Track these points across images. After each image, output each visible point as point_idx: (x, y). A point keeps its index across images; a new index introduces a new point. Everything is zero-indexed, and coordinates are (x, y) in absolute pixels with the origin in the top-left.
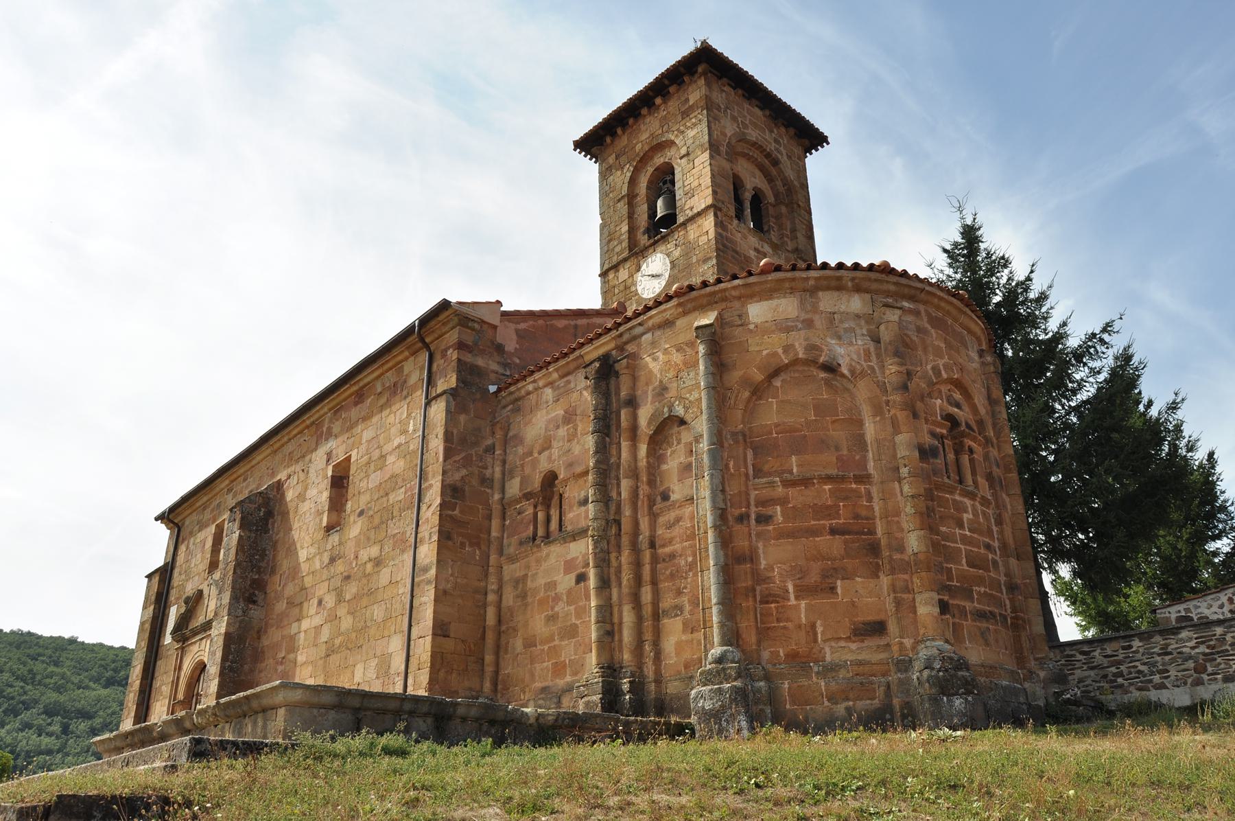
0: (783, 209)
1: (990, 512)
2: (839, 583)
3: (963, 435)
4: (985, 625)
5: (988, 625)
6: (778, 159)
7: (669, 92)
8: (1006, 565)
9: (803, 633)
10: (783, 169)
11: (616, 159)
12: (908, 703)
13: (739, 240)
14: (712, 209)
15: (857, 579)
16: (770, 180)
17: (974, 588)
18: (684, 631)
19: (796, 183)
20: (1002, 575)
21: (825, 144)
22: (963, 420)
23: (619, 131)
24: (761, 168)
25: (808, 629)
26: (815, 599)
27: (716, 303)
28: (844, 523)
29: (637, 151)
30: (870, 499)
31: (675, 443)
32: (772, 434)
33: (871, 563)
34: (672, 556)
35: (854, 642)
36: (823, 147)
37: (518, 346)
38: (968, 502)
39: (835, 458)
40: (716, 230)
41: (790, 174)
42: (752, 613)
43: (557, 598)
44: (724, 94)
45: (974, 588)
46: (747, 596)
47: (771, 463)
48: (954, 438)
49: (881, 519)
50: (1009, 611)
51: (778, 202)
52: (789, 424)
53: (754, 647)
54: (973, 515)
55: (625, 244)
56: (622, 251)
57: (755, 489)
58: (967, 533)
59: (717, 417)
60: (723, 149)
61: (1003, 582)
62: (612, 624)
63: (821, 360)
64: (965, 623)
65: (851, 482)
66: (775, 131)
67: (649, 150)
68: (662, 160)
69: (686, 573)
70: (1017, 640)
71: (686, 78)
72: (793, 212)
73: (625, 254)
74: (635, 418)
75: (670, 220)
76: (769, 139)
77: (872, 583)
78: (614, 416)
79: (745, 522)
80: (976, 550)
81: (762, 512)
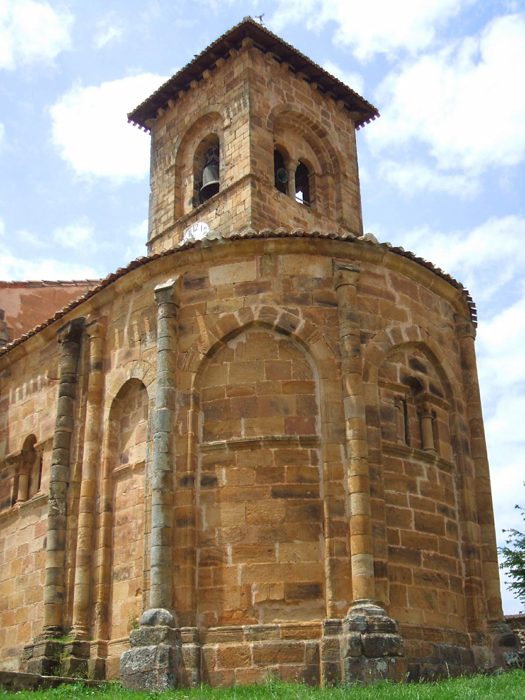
0: (330, 180)
1: (453, 476)
2: (277, 546)
3: (426, 398)
4: (431, 588)
5: (435, 588)
6: (325, 130)
7: (216, 66)
8: (464, 528)
9: (237, 595)
10: (330, 140)
11: (167, 131)
12: (333, 665)
13: (277, 209)
14: (250, 180)
15: (296, 541)
16: (317, 151)
17: (422, 551)
18: (130, 594)
19: (344, 154)
20: (460, 538)
21: (375, 116)
22: (427, 383)
23: (170, 103)
24: (309, 140)
25: (244, 591)
26: (252, 562)
27: (180, 266)
28: (287, 486)
29: (186, 122)
30: (315, 461)
31: (137, 406)
32: (223, 396)
33: (311, 526)
34: (125, 519)
35: (288, 604)
36: (374, 119)
37: (22, 312)
38: (424, 466)
39: (283, 420)
40: (252, 200)
41: (338, 145)
42: (189, 576)
43: (27, 562)
44: (269, 68)
45: (422, 551)
46: (185, 558)
47: (221, 425)
48: (417, 401)
49: (324, 481)
50: (464, 573)
51: (325, 173)
52: (241, 387)
53: (189, 609)
54: (429, 477)
55: (171, 214)
56: (168, 220)
57: (203, 452)
58: (420, 496)
59: (168, 379)
60: (265, 120)
61: (460, 545)
62: (65, 586)
63: (276, 322)
64: (407, 586)
65: (297, 445)
66: (324, 103)
67: (197, 121)
68: (208, 132)
69: (135, 535)
70: (470, 604)
71: (231, 52)
72: (339, 182)
73: (171, 223)
74: (101, 382)
75: (215, 188)
76: (316, 112)
77: (311, 545)
78: (81, 378)
79: (189, 484)
80: (428, 513)
81: (207, 475)
